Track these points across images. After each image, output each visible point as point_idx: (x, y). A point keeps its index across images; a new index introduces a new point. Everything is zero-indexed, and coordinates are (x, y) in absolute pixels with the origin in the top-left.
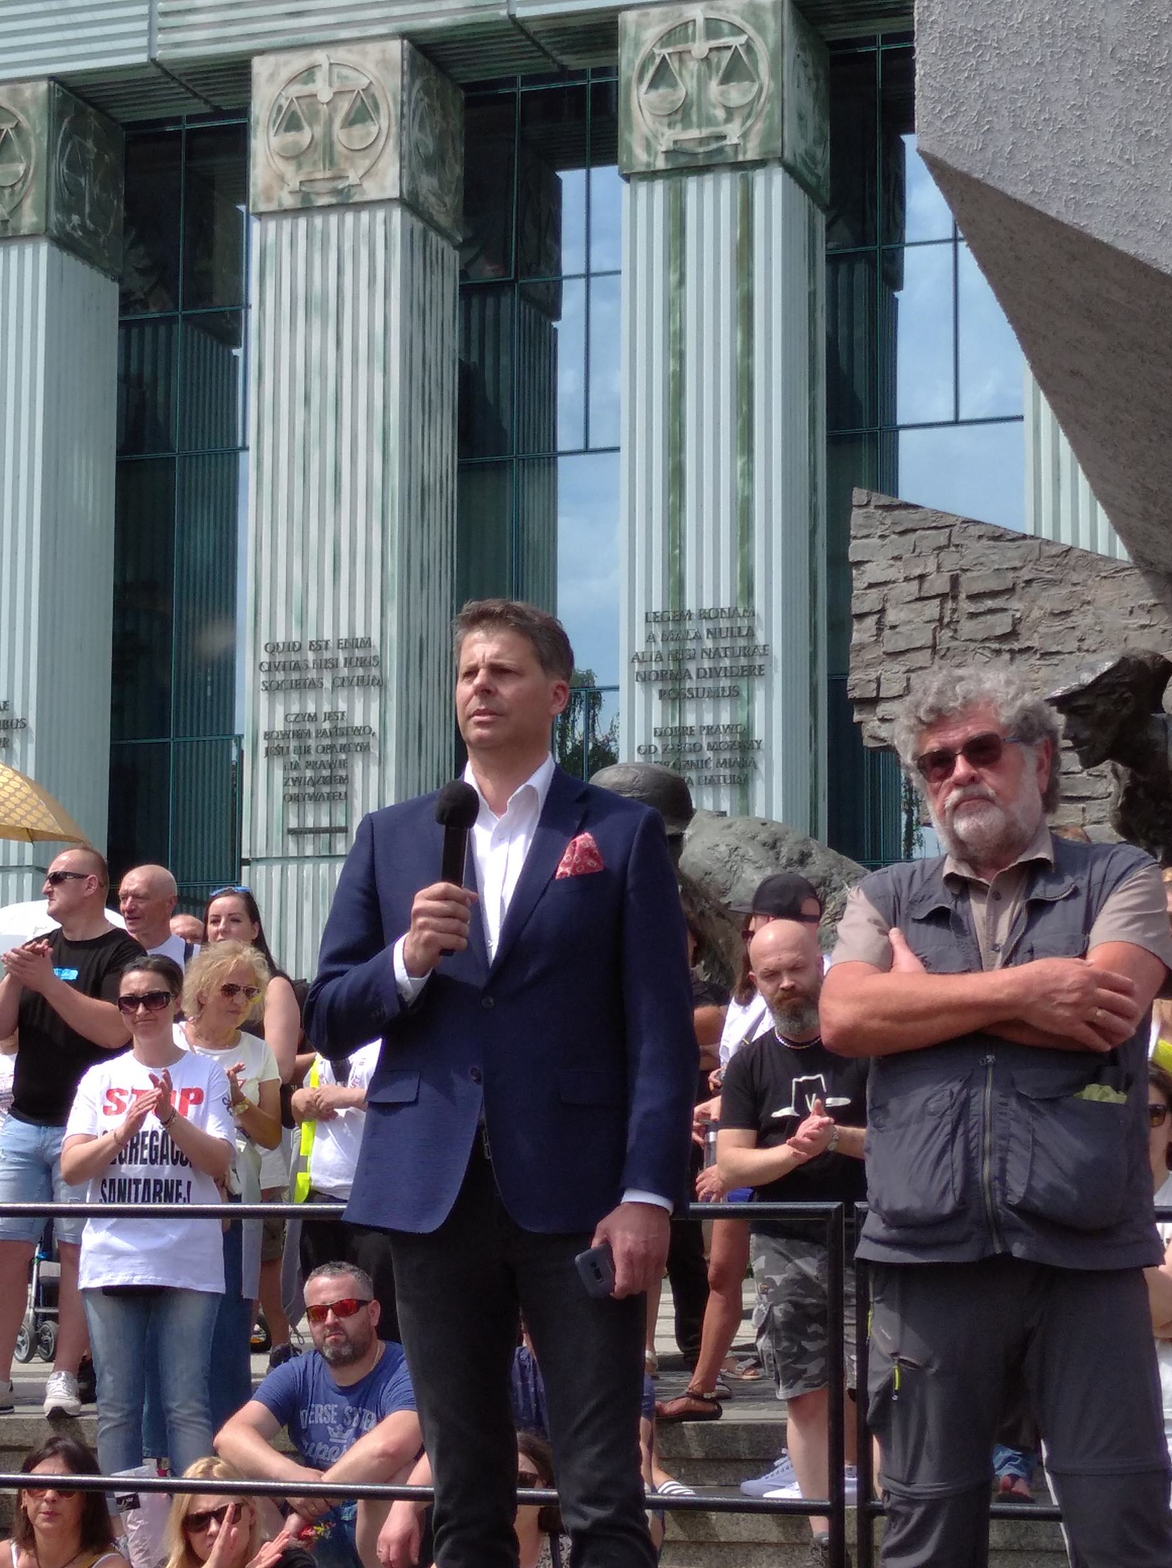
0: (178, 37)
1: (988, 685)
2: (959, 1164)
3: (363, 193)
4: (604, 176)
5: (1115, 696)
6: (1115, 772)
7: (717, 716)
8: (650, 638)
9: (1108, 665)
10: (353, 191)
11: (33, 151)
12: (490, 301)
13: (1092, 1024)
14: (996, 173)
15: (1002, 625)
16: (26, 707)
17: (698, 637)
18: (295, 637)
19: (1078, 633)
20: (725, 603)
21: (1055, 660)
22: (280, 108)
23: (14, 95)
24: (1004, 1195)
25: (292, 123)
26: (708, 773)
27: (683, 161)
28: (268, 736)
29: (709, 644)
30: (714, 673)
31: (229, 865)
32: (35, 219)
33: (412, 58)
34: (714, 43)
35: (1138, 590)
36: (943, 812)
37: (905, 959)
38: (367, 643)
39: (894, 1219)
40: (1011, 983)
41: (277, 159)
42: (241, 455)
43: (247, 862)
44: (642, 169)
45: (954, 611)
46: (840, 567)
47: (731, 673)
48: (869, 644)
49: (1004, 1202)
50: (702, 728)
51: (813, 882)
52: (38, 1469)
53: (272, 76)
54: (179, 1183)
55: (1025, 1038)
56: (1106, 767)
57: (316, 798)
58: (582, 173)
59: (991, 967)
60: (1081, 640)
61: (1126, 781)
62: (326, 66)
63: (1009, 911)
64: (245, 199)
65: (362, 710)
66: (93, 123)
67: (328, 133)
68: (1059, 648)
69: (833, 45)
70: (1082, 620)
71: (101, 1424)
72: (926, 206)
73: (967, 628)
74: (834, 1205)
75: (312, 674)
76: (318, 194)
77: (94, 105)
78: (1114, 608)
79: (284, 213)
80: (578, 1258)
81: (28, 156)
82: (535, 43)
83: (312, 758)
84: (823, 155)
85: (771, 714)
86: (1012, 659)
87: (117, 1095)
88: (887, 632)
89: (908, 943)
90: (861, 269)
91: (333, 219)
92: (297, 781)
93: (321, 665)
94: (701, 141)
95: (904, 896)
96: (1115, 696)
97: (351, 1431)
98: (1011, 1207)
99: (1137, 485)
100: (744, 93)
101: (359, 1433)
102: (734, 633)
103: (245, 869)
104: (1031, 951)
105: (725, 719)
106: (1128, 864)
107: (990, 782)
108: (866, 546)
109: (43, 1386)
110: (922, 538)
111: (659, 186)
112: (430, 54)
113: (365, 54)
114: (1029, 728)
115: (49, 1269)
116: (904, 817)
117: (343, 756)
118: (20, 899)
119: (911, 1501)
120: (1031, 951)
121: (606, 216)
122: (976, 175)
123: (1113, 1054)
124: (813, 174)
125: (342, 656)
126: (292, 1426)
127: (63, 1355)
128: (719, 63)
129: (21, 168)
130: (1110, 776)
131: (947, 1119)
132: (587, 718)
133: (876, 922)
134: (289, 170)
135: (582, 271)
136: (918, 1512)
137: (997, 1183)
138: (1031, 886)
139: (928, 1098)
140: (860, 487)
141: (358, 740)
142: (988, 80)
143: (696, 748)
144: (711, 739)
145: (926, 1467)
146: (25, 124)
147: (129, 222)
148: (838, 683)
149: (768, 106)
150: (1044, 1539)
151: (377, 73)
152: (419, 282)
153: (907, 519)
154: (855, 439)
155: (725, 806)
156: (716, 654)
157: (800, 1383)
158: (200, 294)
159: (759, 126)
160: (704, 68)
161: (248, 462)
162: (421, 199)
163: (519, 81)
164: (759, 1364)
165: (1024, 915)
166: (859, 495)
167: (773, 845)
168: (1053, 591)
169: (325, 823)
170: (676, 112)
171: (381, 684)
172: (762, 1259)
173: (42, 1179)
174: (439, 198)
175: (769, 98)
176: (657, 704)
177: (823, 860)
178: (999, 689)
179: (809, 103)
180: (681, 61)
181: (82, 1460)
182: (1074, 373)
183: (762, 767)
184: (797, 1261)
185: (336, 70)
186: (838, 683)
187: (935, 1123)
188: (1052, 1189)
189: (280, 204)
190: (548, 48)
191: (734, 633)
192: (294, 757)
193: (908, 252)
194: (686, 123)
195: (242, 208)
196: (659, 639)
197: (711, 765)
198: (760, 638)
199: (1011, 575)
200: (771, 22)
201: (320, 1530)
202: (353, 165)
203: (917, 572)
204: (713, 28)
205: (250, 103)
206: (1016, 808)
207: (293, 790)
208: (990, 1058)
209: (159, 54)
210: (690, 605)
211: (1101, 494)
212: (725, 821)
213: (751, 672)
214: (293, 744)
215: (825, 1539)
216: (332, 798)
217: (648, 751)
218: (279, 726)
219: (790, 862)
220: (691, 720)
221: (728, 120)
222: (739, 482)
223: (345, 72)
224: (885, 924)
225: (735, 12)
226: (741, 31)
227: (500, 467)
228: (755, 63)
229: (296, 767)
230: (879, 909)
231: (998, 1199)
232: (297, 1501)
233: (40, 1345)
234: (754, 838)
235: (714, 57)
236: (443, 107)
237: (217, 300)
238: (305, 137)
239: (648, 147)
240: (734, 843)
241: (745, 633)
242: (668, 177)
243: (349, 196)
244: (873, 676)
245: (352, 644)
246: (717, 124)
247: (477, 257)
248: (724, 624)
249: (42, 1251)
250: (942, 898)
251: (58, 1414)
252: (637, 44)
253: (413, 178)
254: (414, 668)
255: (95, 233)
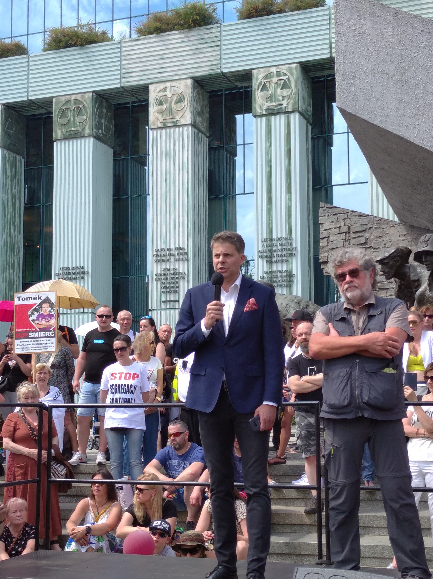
0: (128, 80)
1: (355, 254)
2: (349, 391)
3: (180, 123)
4: (249, 116)
5: (395, 260)
6: (395, 281)
7: (282, 267)
8: (263, 246)
9: (393, 251)
10: (178, 122)
11: (88, 112)
12: (217, 152)
13: (387, 351)
14: (359, 112)
15: (363, 240)
16: (88, 267)
17: (276, 245)
18: (163, 247)
19: (384, 242)
20: (284, 236)
21: (378, 250)
22: (157, 99)
23: (83, 97)
24: (362, 399)
25: (161, 103)
26: (280, 284)
27: (270, 112)
28: (156, 275)
29: (280, 247)
30: (281, 256)
31: (147, 311)
32: (89, 132)
33: (194, 84)
34: (279, 78)
35: (401, 230)
36: (343, 291)
37: (333, 332)
38: (183, 249)
39: (331, 406)
40: (364, 340)
41: (156, 113)
42: (148, 196)
43: (151, 310)
44: (259, 114)
45: (349, 237)
46: (316, 225)
47: (285, 255)
48: (325, 246)
49: (362, 401)
50: (278, 271)
51: (310, 313)
52: (95, 478)
53: (155, 90)
54: (132, 399)
55: (367, 355)
56: (393, 280)
57: (170, 292)
58: (242, 115)
59: (357, 335)
60: (385, 244)
61: (398, 284)
62: (170, 87)
63: (362, 318)
64: (148, 125)
65: (182, 267)
66: (105, 104)
67: (170, 106)
68: (379, 247)
69: (313, 78)
70: (386, 239)
71: (112, 467)
72: (339, 123)
73: (353, 241)
74: (317, 402)
75: (168, 258)
76: (168, 123)
77: (105, 99)
78: (395, 235)
79: (159, 128)
80: (250, 420)
81: (87, 114)
82: (228, 79)
83: (168, 281)
84: (310, 109)
85: (298, 266)
86: (366, 250)
87: (114, 375)
88: (330, 243)
89: (334, 327)
90: (321, 141)
91: (172, 130)
92: (164, 288)
93: (170, 255)
94: (276, 106)
95: (333, 313)
96: (395, 260)
97: (181, 468)
98: (364, 403)
99: (401, 200)
100: (288, 92)
101: (184, 468)
102: (286, 244)
103: (150, 312)
104: (369, 330)
105: (285, 269)
106: (397, 304)
107: (357, 282)
108: (324, 219)
109: (96, 456)
110: (339, 216)
111: (264, 119)
112: (199, 83)
113: (180, 84)
114: (368, 266)
115: (97, 424)
116: (336, 296)
117: (177, 280)
118: (88, 322)
119: (337, 485)
120: (369, 330)
121: (247, 126)
122: (353, 113)
123: (393, 358)
124: (307, 114)
125: (176, 252)
126: (165, 466)
127: (101, 447)
128: (280, 84)
129: (85, 117)
130: (394, 282)
131: (345, 378)
132: (245, 269)
133: (325, 321)
134: (160, 116)
135: (243, 143)
136: (339, 488)
137: (360, 396)
138: (369, 311)
139: (340, 372)
140: (322, 202)
141: (181, 276)
142: (356, 86)
143: (277, 277)
144: (281, 274)
145: (341, 476)
146: (86, 105)
147: (115, 132)
148: (316, 258)
149: (294, 95)
150: (378, 497)
151: (184, 89)
152: (196, 145)
153: (335, 211)
154: (320, 189)
155: (285, 293)
156: (281, 250)
157: (309, 453)
158: (136, 151)
159: (292, 101)
160: (276, 85)
161: (149, 198)
162: (197, 124)
163: (224, 90)
164: (297, 449)
165: (367, 319)
166: (322, 204)
167: (298, 303)
168: (377, 230)
169: (172, 299)
170: (268, 98)
171: (187, 260)
172: (298, 418)
173: (94, 398)
174: (202, 124)
175: (295, 94)
176: (265, 264)
177: (312, 307)
178: (357, 255)
179: (306, 95)
180: (269, 84)
181: (107, 475)
182: (383, 169)
183: (295, 281)
184: (309, 419)
185: (172, 88)
186: (316, 258)
187: (342, 379)
188: (375, 398)
189: (157, 126)
190: (232, 81)
191: (286, 244)
192: (163, 281)
193: (334, 136)
194: (271, 101)
195: (147, 127)
196: (266, 246)
197: (281, 281)
198: (294, 246)
199: (365, 226)
200: (295, 72)
201: (174, 495)
202: (178, 114)
203: (338, 226)
204: (278, 74)
205: (148, 98)
206: (364, 289)
207: (163, 290)
208: (357, 361)
209: (123, 85)
210: (274, 236)
211: (391, 203)
212: (285, 296)
213: (291, 255)
214: (163, 277)
215: (316, 497)
216: (174, 292)
217: (263, 278)
218: (159, 272)
219: (303, 308)
220: (275, 269)
221: (283, 100)
222: (288, 202)
223: (175, 88)
224: (327, 321)
225: (285, 70)
226: (286, 75)
227: (220, 198)
228: (290, 83)
229: (164, 283)
230: (326, 318)
231: (360, 401)
232: (167, 487)
233: (95, 445)
234: (293, 301)
235: (279, 82)
236: (202, 98)
237: (140, 153)
238: (164, 107)
239: (261, 108)
240: (287, 302)
241: (290, 244)
242: (266, 116)
243: (176, 123)
244: (326, 255)
245: (179, 249)
246: (280, 101)
247: (212, 140)
248: (284, 242)
249: (95, 419)
250: (343, 314)
251: (100, 464)
252: (257, 79)
253: (194, 118)
254: (197, 256)
255: (106, 135)
